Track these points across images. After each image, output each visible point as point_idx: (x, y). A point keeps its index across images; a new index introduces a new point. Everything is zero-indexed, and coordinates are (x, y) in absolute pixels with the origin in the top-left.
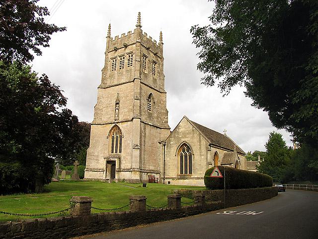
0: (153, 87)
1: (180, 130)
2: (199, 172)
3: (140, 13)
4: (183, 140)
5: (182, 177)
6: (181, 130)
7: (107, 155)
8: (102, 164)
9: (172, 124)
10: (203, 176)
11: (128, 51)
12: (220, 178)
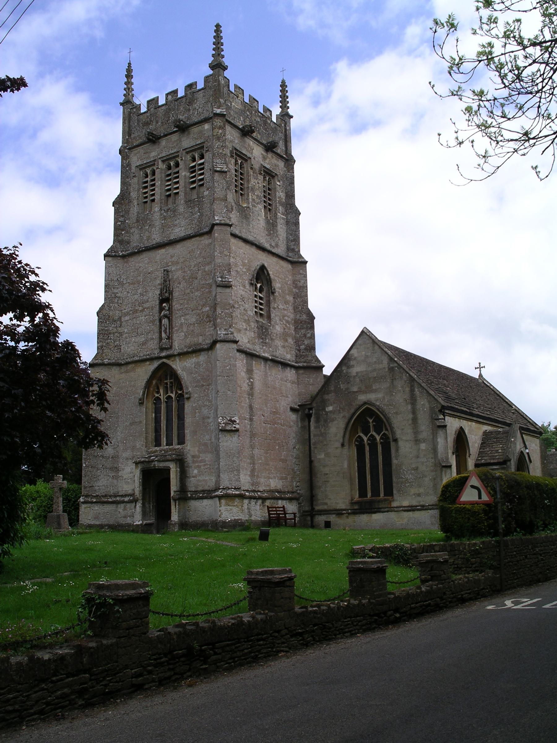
0: (267, 246)
1: (354, 371)
2: (413, 491)
3: (218, 26)
4: (362, 398)
5: (365, 507)
6: (357, 369)
7: (142, 452)
8: (130, 480)
9: (329, 357)
10: (432, 499)
11: (187, 142)
12: (487, 504)
